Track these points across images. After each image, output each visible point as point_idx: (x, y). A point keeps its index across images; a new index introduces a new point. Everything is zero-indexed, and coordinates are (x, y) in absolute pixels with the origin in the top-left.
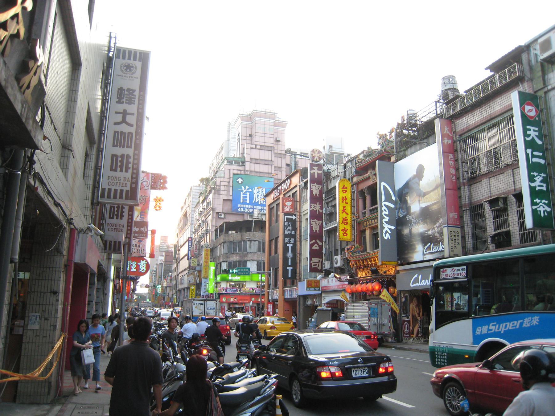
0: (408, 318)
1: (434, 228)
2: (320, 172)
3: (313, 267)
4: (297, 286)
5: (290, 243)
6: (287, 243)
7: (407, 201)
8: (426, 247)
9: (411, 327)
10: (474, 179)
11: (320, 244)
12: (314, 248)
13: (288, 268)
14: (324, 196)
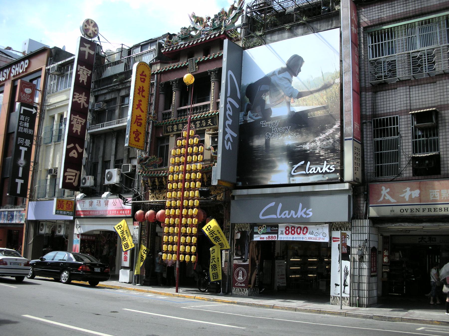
0: (245, 261)
1: (314, 141)
2: (92, 53)
3: (67, 181)
4: (24, 206)
5: (24, 146)
6: (20, 145)
7: (264, 101)
8: (296, 166)
9: (249, 275)
10: (380, 86)
11: (80, 150)
12: (72, 154)
13: (17, 180)
14: (92, 85)
